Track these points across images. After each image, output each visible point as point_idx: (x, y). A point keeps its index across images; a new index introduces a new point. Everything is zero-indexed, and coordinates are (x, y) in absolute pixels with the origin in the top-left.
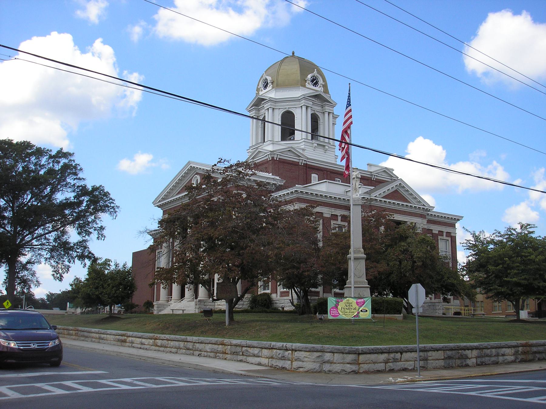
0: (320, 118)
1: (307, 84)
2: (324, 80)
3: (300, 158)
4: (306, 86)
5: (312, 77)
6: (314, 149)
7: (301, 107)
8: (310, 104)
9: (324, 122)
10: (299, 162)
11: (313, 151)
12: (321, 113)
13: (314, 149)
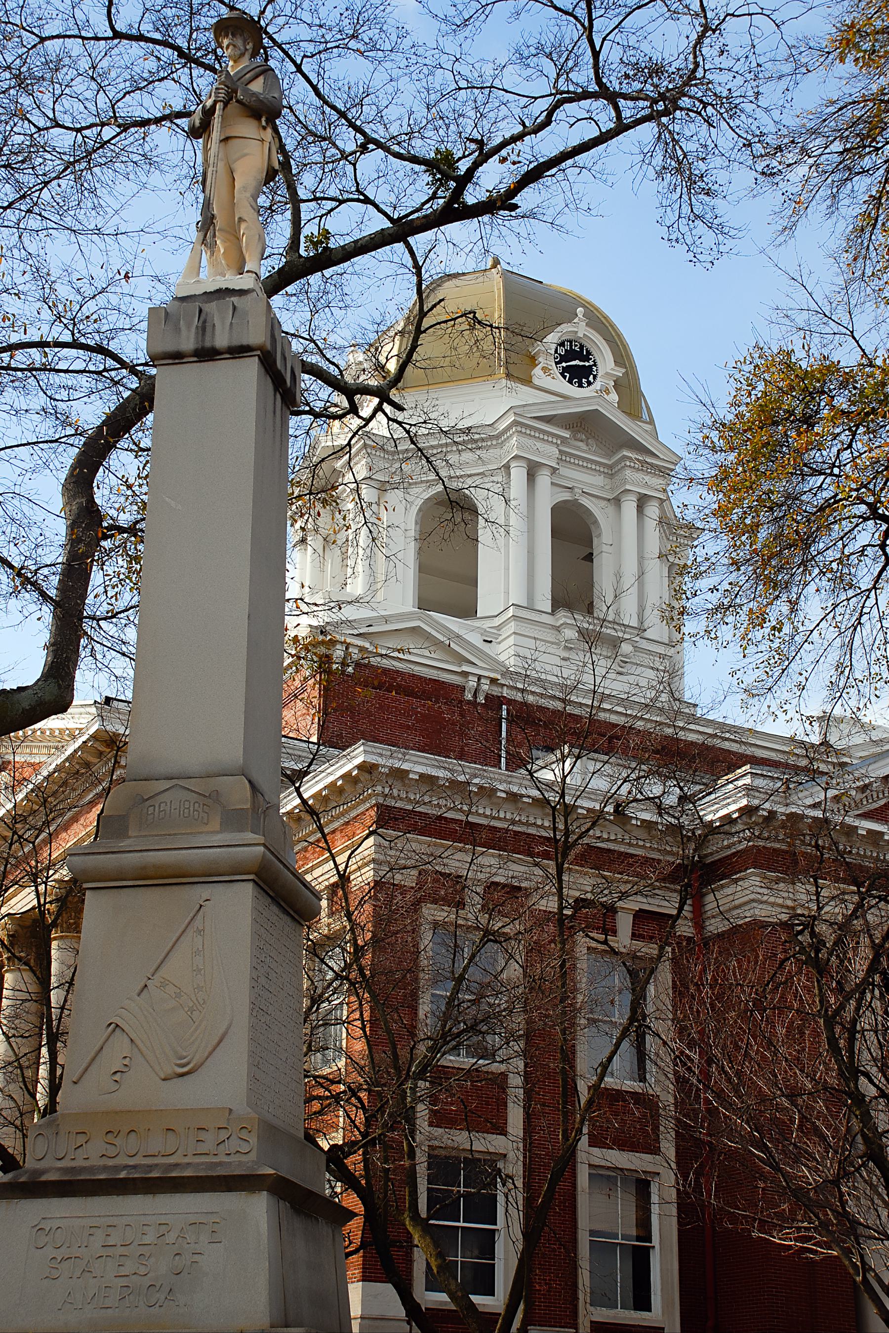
0: (599, 526)
1: (537, 371)
2: (622, 356)
3: (466, 668)
4: (536, 381)
5: (562, 344)
6: (565, 654)
7: (507, 467)
8: (547, 453)
9: (617, 545)
10: (463, 689)
11: (558, 662)
12: (603, 503)
13: (565, 654)
